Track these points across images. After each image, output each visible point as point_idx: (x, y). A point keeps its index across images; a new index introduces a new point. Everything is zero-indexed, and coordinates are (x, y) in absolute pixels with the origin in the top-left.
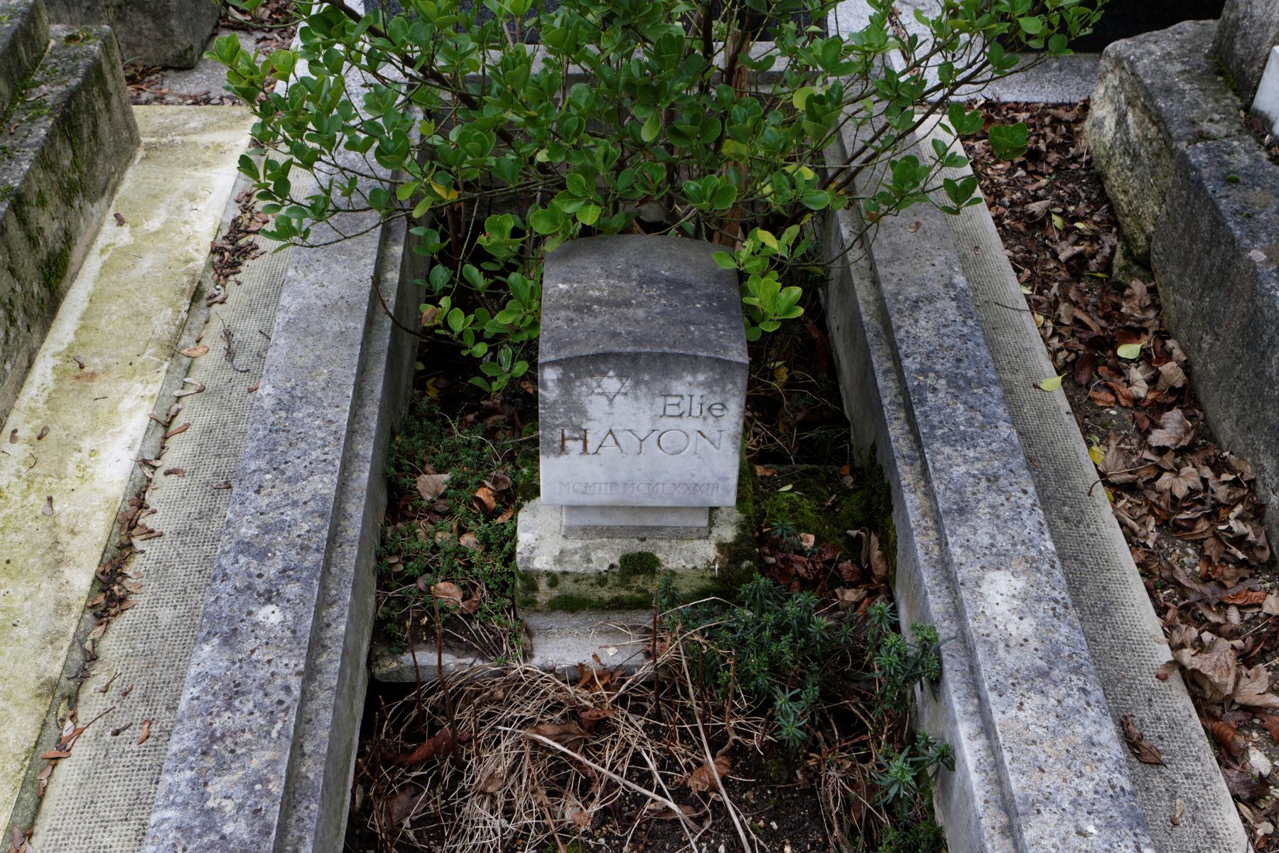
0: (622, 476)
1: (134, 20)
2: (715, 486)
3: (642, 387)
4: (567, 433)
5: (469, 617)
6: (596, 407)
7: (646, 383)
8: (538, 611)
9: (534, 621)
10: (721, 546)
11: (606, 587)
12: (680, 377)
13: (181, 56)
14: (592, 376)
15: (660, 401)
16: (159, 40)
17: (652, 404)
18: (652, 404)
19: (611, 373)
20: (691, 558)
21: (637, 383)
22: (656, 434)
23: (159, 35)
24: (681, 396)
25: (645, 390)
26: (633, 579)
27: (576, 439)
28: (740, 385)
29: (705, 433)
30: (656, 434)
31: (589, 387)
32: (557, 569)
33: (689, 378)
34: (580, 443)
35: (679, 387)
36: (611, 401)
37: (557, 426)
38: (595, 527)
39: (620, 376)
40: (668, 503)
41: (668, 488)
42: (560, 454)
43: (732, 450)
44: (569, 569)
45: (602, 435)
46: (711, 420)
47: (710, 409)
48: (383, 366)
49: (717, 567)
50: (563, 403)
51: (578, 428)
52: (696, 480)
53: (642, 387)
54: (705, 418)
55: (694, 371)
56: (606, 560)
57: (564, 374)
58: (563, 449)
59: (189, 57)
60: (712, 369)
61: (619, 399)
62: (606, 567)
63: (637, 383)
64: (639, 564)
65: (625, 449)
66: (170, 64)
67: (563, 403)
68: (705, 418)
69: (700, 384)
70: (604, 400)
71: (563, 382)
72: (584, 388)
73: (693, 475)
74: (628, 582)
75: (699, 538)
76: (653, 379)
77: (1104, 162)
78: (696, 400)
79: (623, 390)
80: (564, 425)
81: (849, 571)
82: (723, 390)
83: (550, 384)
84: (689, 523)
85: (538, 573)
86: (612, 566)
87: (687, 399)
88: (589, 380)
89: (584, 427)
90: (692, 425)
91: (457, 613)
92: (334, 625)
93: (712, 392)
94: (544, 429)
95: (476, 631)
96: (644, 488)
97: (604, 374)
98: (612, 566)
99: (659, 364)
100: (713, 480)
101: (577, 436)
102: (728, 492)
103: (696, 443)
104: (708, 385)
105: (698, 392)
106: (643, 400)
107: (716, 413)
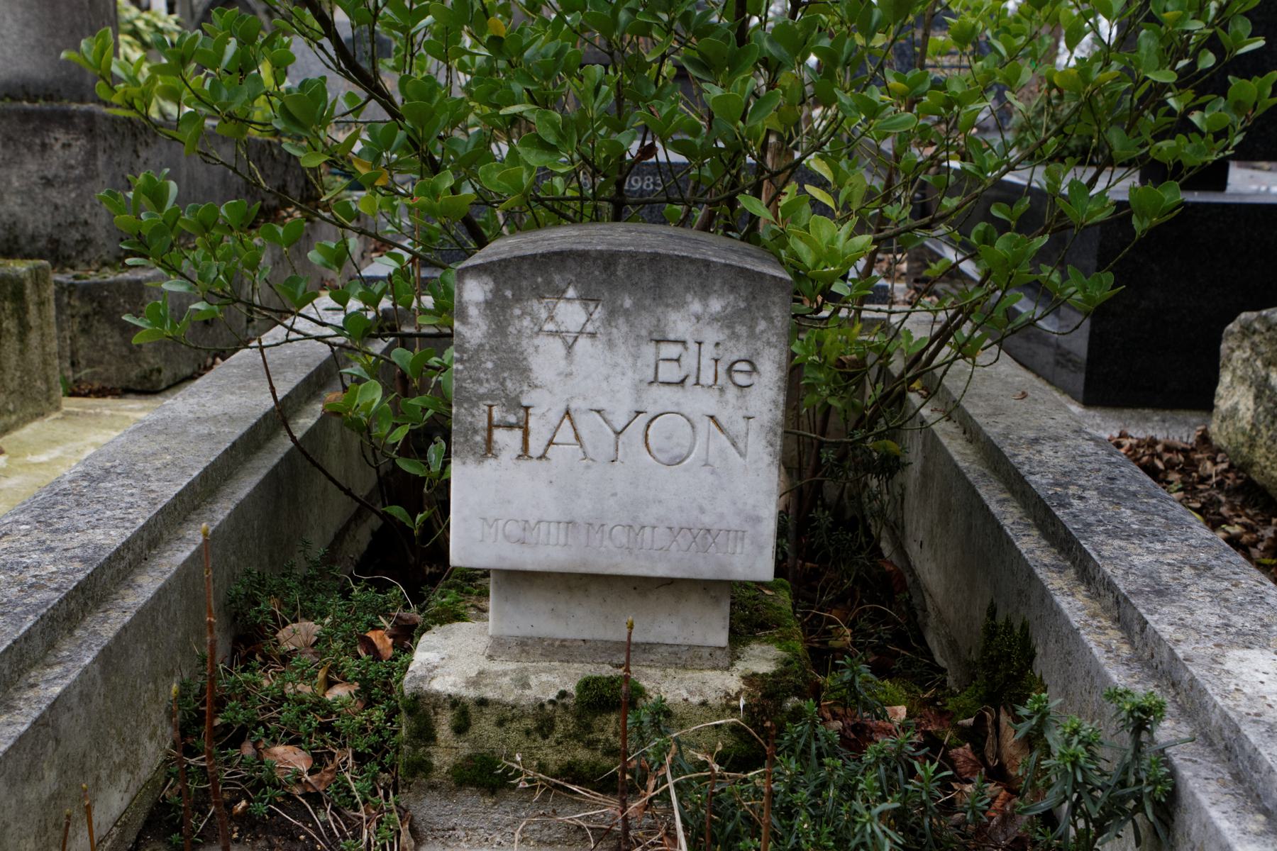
0: (583, 508)
1: (101, 332)
2: (740, 535)
3: (621, 321)
4: (497, 414)
5: (316, 799)
6: (545, 358)
7: (627, 313)
8: (433, 787)
9: (430, 809)
10: (750, 679)
11: (551, 740)
12: (680, 305)
13: (145, 377)
14: (541, 297)
15: (649, 350)
16: (123, 357)
17: (636, 357)
18: (636, 357)
19: (571, 293)
20: (702, 682)
21: (613, 313)
22: (642, 420)
23: (125, 351)
24: (684, 342)
25: (624, 328)
26: (598, 722)
27: (510, 427)
28: (778, 323)
29: (723, 420)
30: (642, 420)
31: (535, 319)
32: (471, 694)
33: (696, 307)
34: (518, 433)
35: (680, 324)
36: (569, 348)
37: (481, 397)
38: (541, 640)
39: (585, 299)
40: (661, 571)
41: (662, 536)
42: (485, 456)
43: (767, 459)
44: (490, 694)
45: (554, 417)
46: (732, 392)
47: (730, 370)
48: (261, 477)
49: (742, 702)
50: (493, 350)
51: (514, 404)
52: (707, 520)
53: (621, 321)
54: (722, 390)
55: (705, 293)
56: (553, 685)
57: (497, 292)
58: (489, 449)
59: (154, 378)
60: (733, 289)
61: (583, 342)
62: (552, 695)
63: (612, 314)
64: (605, 699)
65: (589, 449)
66: (131, 386)
67: (493, 350)
68: (722, 390)
69: (715, 319)
70: (556, 346)
71: (496, 308)
72: (526, 322)
73: (702, 511)
74: (588, 728)
75: (714, 668)
76: (639, 306)
77: (1245, 450)
78: (708, 351)
79: (590, 328)
80: (491, 395)
81: (967, 760)
82: (752, 335)
83: (473, 312)
84: (697, 640)
85: (438, 701)
86: (563, 694)
87: (693, 347)
88: (535, 304)
89: (525, 402)
90: (700, 402)
91: (297, 791)
92: (43, 686)
93: (734, 336)
94: (460, 405)
95: (325, 824)
96: (621, 536)
97: (559, 294)
98: (563, 694)
99: (647, 277)
100: (734, 522)
101: (512, 419)
102: (761, 548)
103: (712, 443)
104: (727, 321)
105: (712, 335)
106: (622, 349)
107: (741, 379)
